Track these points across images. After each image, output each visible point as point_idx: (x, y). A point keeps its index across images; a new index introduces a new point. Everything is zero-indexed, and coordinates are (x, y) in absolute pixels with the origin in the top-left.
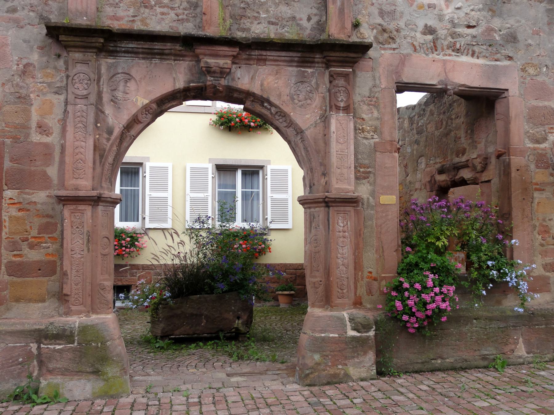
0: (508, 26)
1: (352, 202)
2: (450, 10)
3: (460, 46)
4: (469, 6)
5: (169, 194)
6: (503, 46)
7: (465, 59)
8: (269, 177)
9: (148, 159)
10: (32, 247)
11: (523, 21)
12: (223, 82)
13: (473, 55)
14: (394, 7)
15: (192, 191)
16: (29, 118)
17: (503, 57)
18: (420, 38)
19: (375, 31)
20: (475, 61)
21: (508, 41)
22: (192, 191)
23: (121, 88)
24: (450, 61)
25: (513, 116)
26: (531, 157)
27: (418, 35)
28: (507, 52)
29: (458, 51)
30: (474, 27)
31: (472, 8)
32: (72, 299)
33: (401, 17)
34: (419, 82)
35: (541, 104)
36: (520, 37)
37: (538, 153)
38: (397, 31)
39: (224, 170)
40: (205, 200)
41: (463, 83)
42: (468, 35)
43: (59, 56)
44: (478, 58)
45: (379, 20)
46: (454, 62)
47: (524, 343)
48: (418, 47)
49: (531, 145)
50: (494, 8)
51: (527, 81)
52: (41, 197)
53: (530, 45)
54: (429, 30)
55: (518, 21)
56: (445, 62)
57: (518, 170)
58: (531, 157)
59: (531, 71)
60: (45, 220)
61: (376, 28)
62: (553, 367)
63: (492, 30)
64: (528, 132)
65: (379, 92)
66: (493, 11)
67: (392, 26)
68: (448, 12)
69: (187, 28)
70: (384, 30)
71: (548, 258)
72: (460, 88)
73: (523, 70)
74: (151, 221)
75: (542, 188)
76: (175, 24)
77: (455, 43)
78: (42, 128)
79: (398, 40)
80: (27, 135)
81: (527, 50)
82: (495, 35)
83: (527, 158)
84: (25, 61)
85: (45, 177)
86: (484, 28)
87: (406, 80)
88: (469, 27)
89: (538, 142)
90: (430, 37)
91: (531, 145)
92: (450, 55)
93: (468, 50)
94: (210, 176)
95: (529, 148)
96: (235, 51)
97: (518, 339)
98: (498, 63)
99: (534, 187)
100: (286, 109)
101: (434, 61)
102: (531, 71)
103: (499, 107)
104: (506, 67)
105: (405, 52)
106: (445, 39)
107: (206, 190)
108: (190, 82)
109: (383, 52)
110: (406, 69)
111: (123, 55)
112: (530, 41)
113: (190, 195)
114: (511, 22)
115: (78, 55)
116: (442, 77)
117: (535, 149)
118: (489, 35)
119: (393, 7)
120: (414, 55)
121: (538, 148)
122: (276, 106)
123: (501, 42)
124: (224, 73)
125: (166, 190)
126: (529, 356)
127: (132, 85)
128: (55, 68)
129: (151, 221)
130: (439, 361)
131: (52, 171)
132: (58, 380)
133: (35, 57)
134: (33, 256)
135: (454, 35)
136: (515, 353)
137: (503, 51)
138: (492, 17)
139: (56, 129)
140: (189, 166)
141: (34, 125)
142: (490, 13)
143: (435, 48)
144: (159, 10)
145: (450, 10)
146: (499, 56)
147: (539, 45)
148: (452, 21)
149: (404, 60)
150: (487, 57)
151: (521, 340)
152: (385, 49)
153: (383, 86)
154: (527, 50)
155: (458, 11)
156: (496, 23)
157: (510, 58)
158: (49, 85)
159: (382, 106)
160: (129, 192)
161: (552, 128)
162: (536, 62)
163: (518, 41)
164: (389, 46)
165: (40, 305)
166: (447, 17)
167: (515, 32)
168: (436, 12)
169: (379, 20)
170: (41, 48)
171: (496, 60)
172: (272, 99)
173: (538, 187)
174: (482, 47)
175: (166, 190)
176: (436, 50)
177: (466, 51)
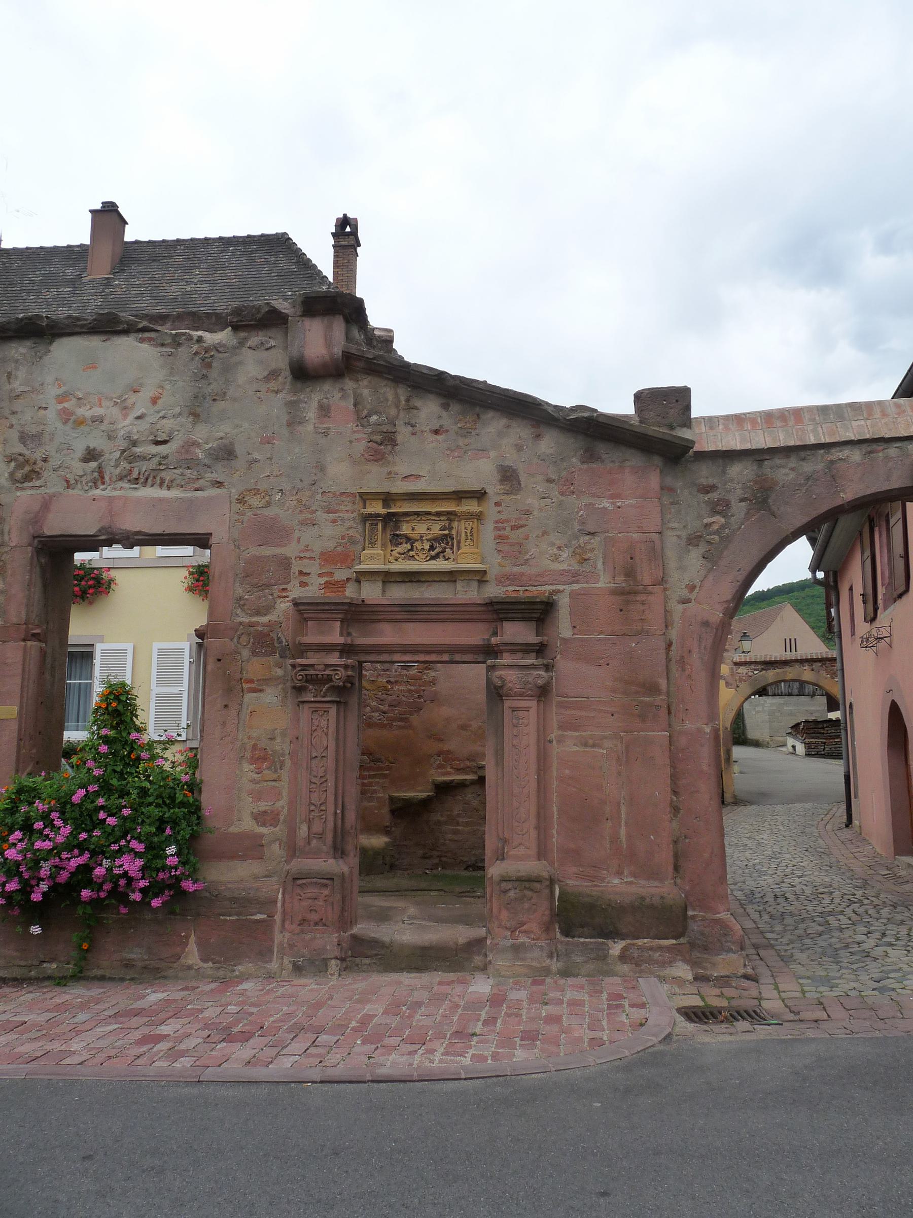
0: (221, 434)
2: (127, 422)
3: (139, 474)
4: (158, 412)
6: (209, 467)
9: (102, 639)
11: (246, 425)
13: (161, 485)
14: (42, 427)
15: (159, 684)
17: (209, 484)
18: (78, 467)
19: (13, 464)
20: (164, 493)
21: (217, 459)
22: (159, 684)
24: (119, 498)
25: (217, 574)
26: (244, 639)
28: (214, 475)
30: (165, 442)
31: (161, 414)
33: (51, 440)
34: (74, 533)
35: (267, 551)
36: (239, 450)
37: (257, 630)
38: (45, 460)
40: (180, 695)
41: (138, 530)
42: (154, 456)
44: (169, 488)
45: (20, 448)
46: (126, 498)
47: (199, 944)
48: (72, 482)
49: (246, 619)
50: (198, 410)
51: (246, 518)
53: (256, 461)
54: (91, 455)
55: (237, 426)
56: (111, 499)
57: (219, 660)
58: (244, 639)
61: (15, 460)
62: (4, 1017)
63: (195, 444)
64: (241, 598)
65: (6, 552)
66: (196, 415)
67: (38, 455)
68: (126, 425)
70: (27, 461)
71: (263, 803)
72: (136, 537)
75: (261, 688)
77: (130, 472)
79: (45, 474)
81: (249, 468)
82: (197, 451)
83: (235, 640)
86: (181, 443)
87: (48, 532)
88: (157, 443)
89: (258, 613)
90: (94, 464)
92: (121, 488)
93: (154, 477)
95: (241, 623)
97: (188, 937)
98: (199, 494)
99: (245, 686)
101: (94, 500)
102: (255, 501)
105: (52, 491)
106: (116, 466)
109: (18, 493)
110: (51, 516)
111: (433, 518)
112: (256, 455)
113: (156, 690)
114: (225, 429)
116: (105, 523)
117: (251, 625)
118: (187, 451)
119: (40, 428)
121: (257, 624)
123: (206, 461)
126: (205, 965)
130: (54, 966)
135: (133, 459)
136: (182, 960)
137: (209, 475)
138: (194, 424)
140: (156, 645)
142: (191, 419)
143: (99, 479)
145: (127, 422)
146: (201, 483)
147: (271, 459)
148: (128, 437)
149: (46, 505)
150: (182, 486)
151: (193, 938)
152: (23, 489)
153: (13, 544)
154: (249, 468)
155: (139, 422)
156: (201, 433)
157: (219, 484)
159: (9, 572)
160: (82, 686)
161: (284, 589)
162: (262, 487)
163: (236, 457)
164: (31, 484)
166: (122, 432)
167: (232, 444)
168: (104, 427)
169: (19, 448)
171: (197, 490)
173: (253, 686)
174: (176, 471)
176: (103, 483)
177: (150, 480)
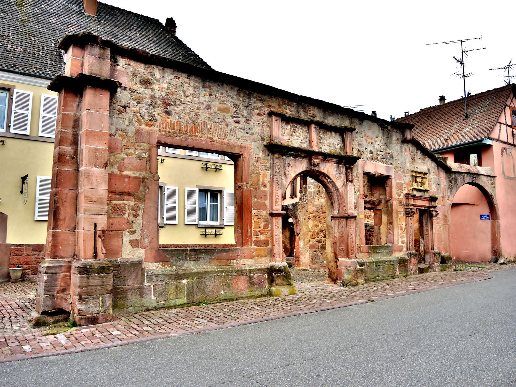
1: (354, 217)
5: (176, 205)
7: (380, 163)
8: (225, 197)
9: (165, 184)
10: (261, 234)
12: (317, 169)
15: (188, 203)
16: (259, 180)
22: (188, 203)
23: (287, 169)
27: (368, 154)
29: (378, 160)
32: (276, 255)
36: (394, 157)
39: (203, 191)
43: (268, 155)
45: (358, 147)
49: (398, 197)
52: (264, 213)
59: (397, 169)
60: (266, 223)
69: (305, 146)
73: (395, 169)
74: (167, 220)
76: (301, 144)
78: (264, 186)
80: (259, 187)
84: (257, 156)
85: (265, 205)
88: (381, 151)
90: (371, 155)
91: (398, 197)
94: (197, 195)
96: (321, 157)
100: (334, 180)
103: (388, 182)
104: (391, 167)
107: (195, 203)
108: (307, 168)
113: (187, 205)
115: (276, 155)
120: (368, 161)
122: (330, 179)
124: (318, 165)
125: (175, 202)
127: (290, 168)
128: (267, 160)
129: (167, 220)
131: (267, 203)
132: (278, 288)
133: (261, 155)
134: (262, 238)
139: (268, 185)
140: (187, 189)
141: (261, 183)
143: (372, 159)
144: (296, 138)
157: (391, 164)
158: (265, 166)
165: (265, 258)
169: (358, 147)
170: (263, 151)
172: (330, 176)
175: (175, 202)
